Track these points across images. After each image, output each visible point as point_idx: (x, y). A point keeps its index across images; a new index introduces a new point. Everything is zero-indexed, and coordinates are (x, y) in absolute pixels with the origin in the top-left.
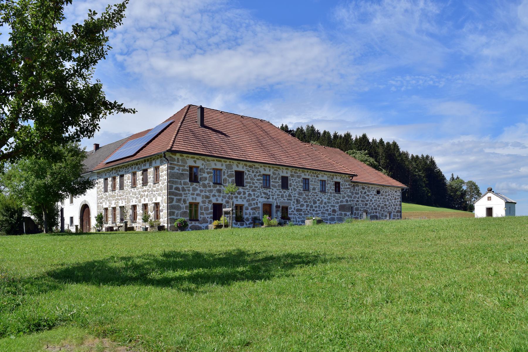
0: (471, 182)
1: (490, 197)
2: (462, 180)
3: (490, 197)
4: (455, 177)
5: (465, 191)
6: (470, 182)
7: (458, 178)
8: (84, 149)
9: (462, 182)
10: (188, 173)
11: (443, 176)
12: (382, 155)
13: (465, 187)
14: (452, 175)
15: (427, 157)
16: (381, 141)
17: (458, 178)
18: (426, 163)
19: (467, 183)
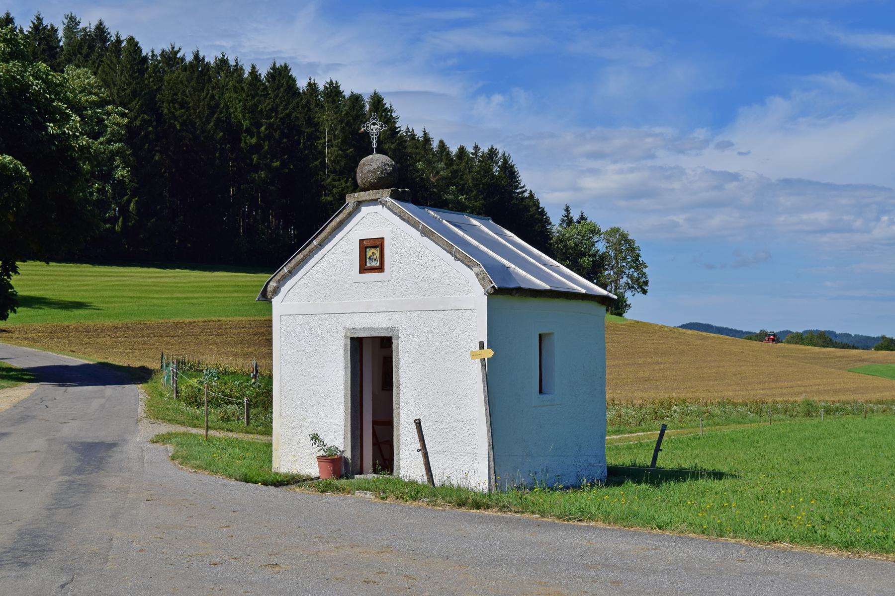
0: (618, 230)
1: (378, 244)
2: (595, 226)
3: (378, 244)
4: (575, 215)
5: (603, 257)
6: (615, 231)
7: (582, 218)
8: (173, 48)
9: (595, 231)
10: (608, 363)
11: (543, 213)
12: (332, 131)
13: (601, 247)
14: (567, 209)
15: (492, 153)
16: (137, 43)
17: (582, 218)
18: (488, 171)
19: (606, 232)
